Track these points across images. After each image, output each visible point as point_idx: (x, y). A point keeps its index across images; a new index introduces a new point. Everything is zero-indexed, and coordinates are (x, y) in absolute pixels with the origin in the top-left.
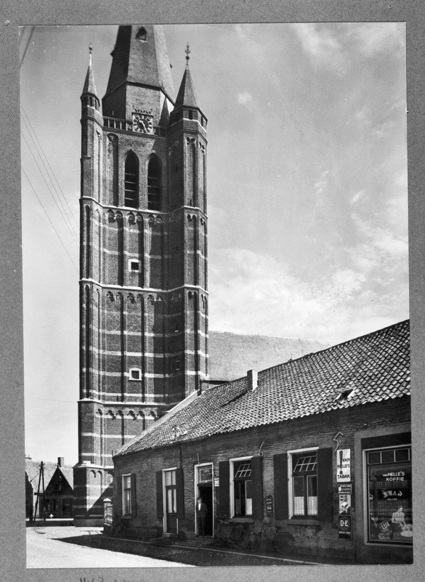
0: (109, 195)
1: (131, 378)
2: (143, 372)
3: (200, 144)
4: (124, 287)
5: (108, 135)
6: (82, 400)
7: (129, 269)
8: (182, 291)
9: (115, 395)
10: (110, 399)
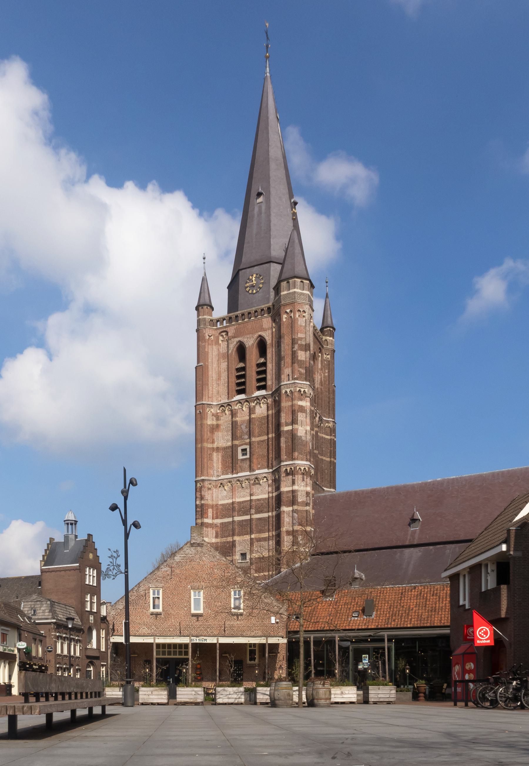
5: (220, 333)
7: (240, 457)
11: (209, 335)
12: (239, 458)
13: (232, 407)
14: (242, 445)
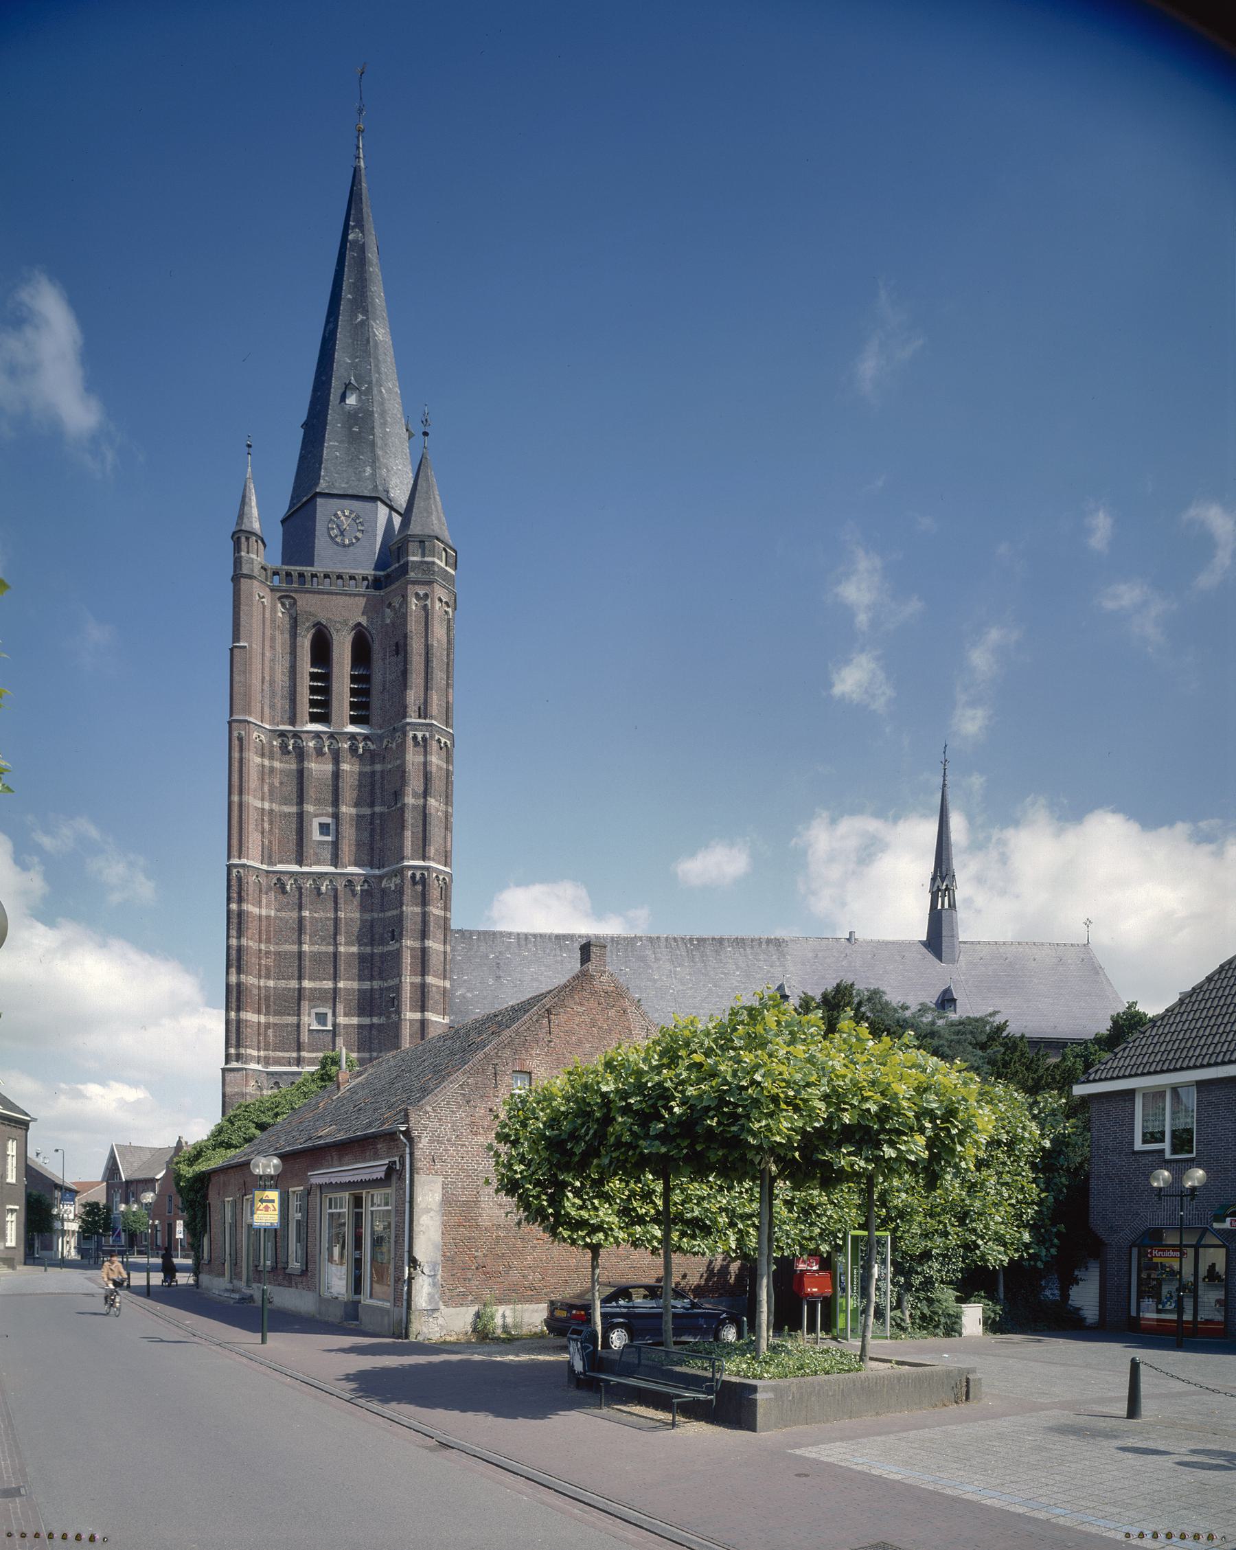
0: (281, 703)
1: (315, 1027)
2: (334, 1014)
3: (440, 600)
4: (305, 869)
5: (280, 598)
6: (228, 1066)
7: (316, 835)
8: (400, 872)
9: (286, 1055)
10: (278, 1062)
11: (259, 596)
12: (314, 839)
13: (302, 741)
14: (322, 815)
